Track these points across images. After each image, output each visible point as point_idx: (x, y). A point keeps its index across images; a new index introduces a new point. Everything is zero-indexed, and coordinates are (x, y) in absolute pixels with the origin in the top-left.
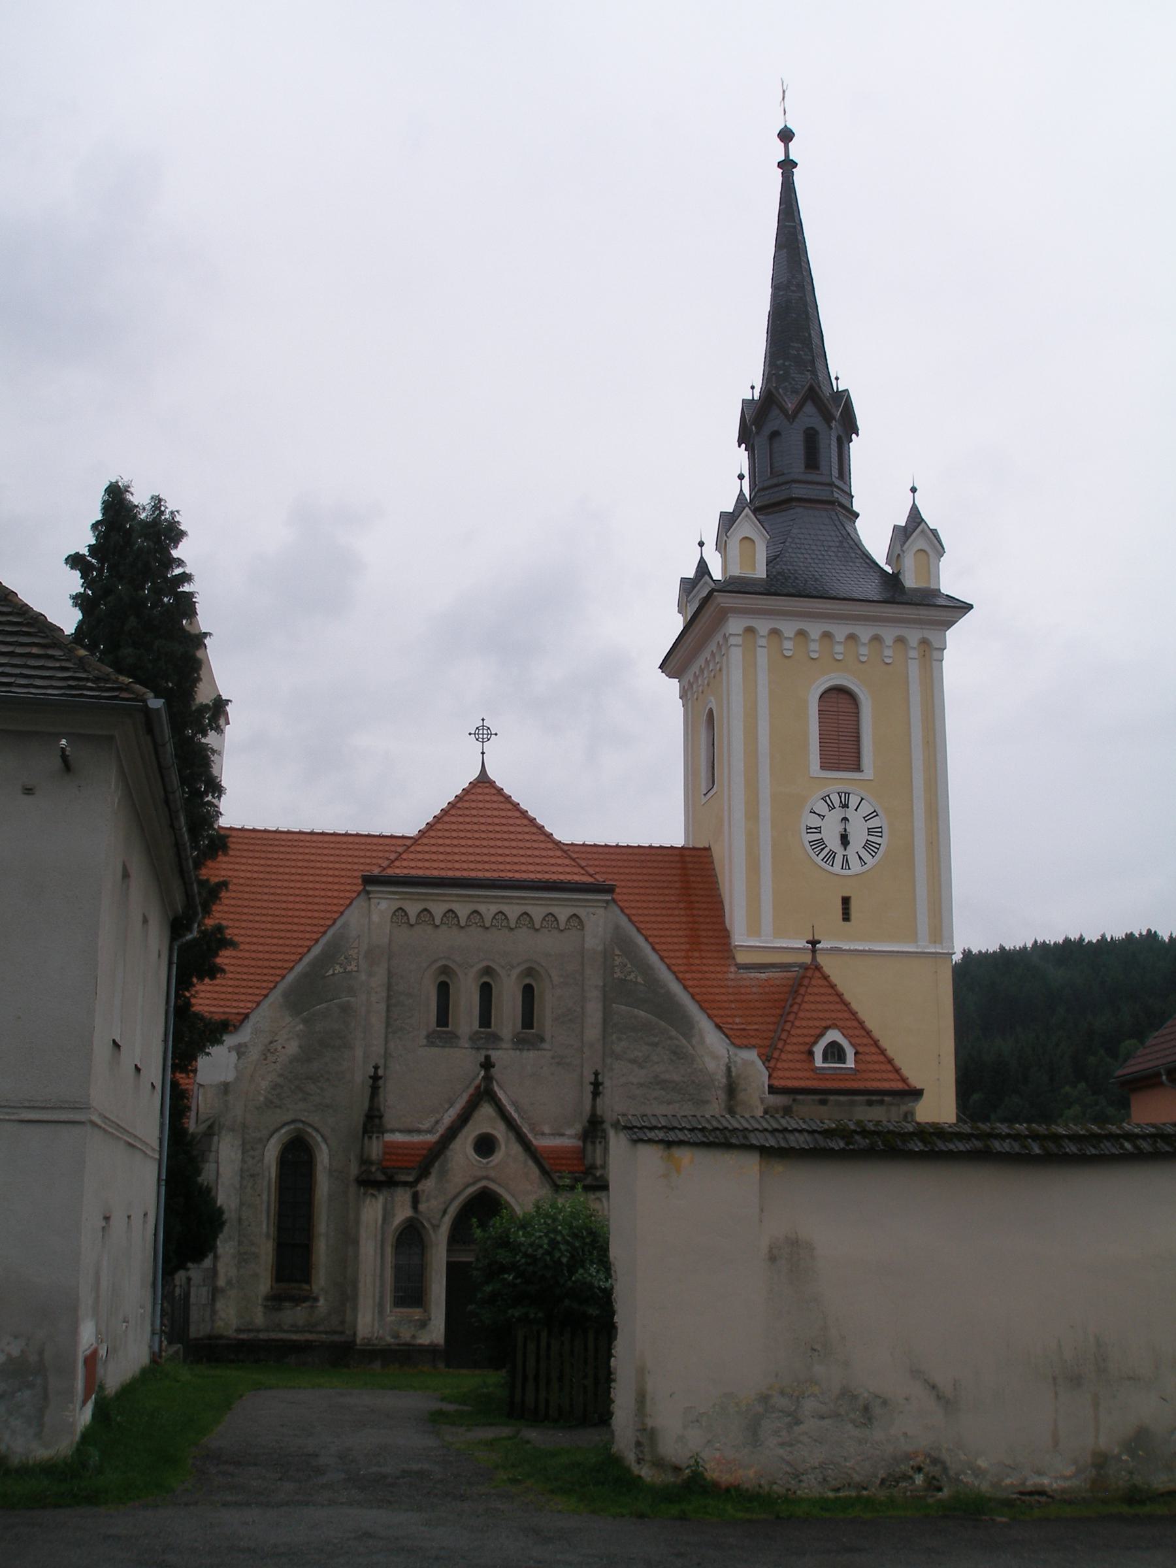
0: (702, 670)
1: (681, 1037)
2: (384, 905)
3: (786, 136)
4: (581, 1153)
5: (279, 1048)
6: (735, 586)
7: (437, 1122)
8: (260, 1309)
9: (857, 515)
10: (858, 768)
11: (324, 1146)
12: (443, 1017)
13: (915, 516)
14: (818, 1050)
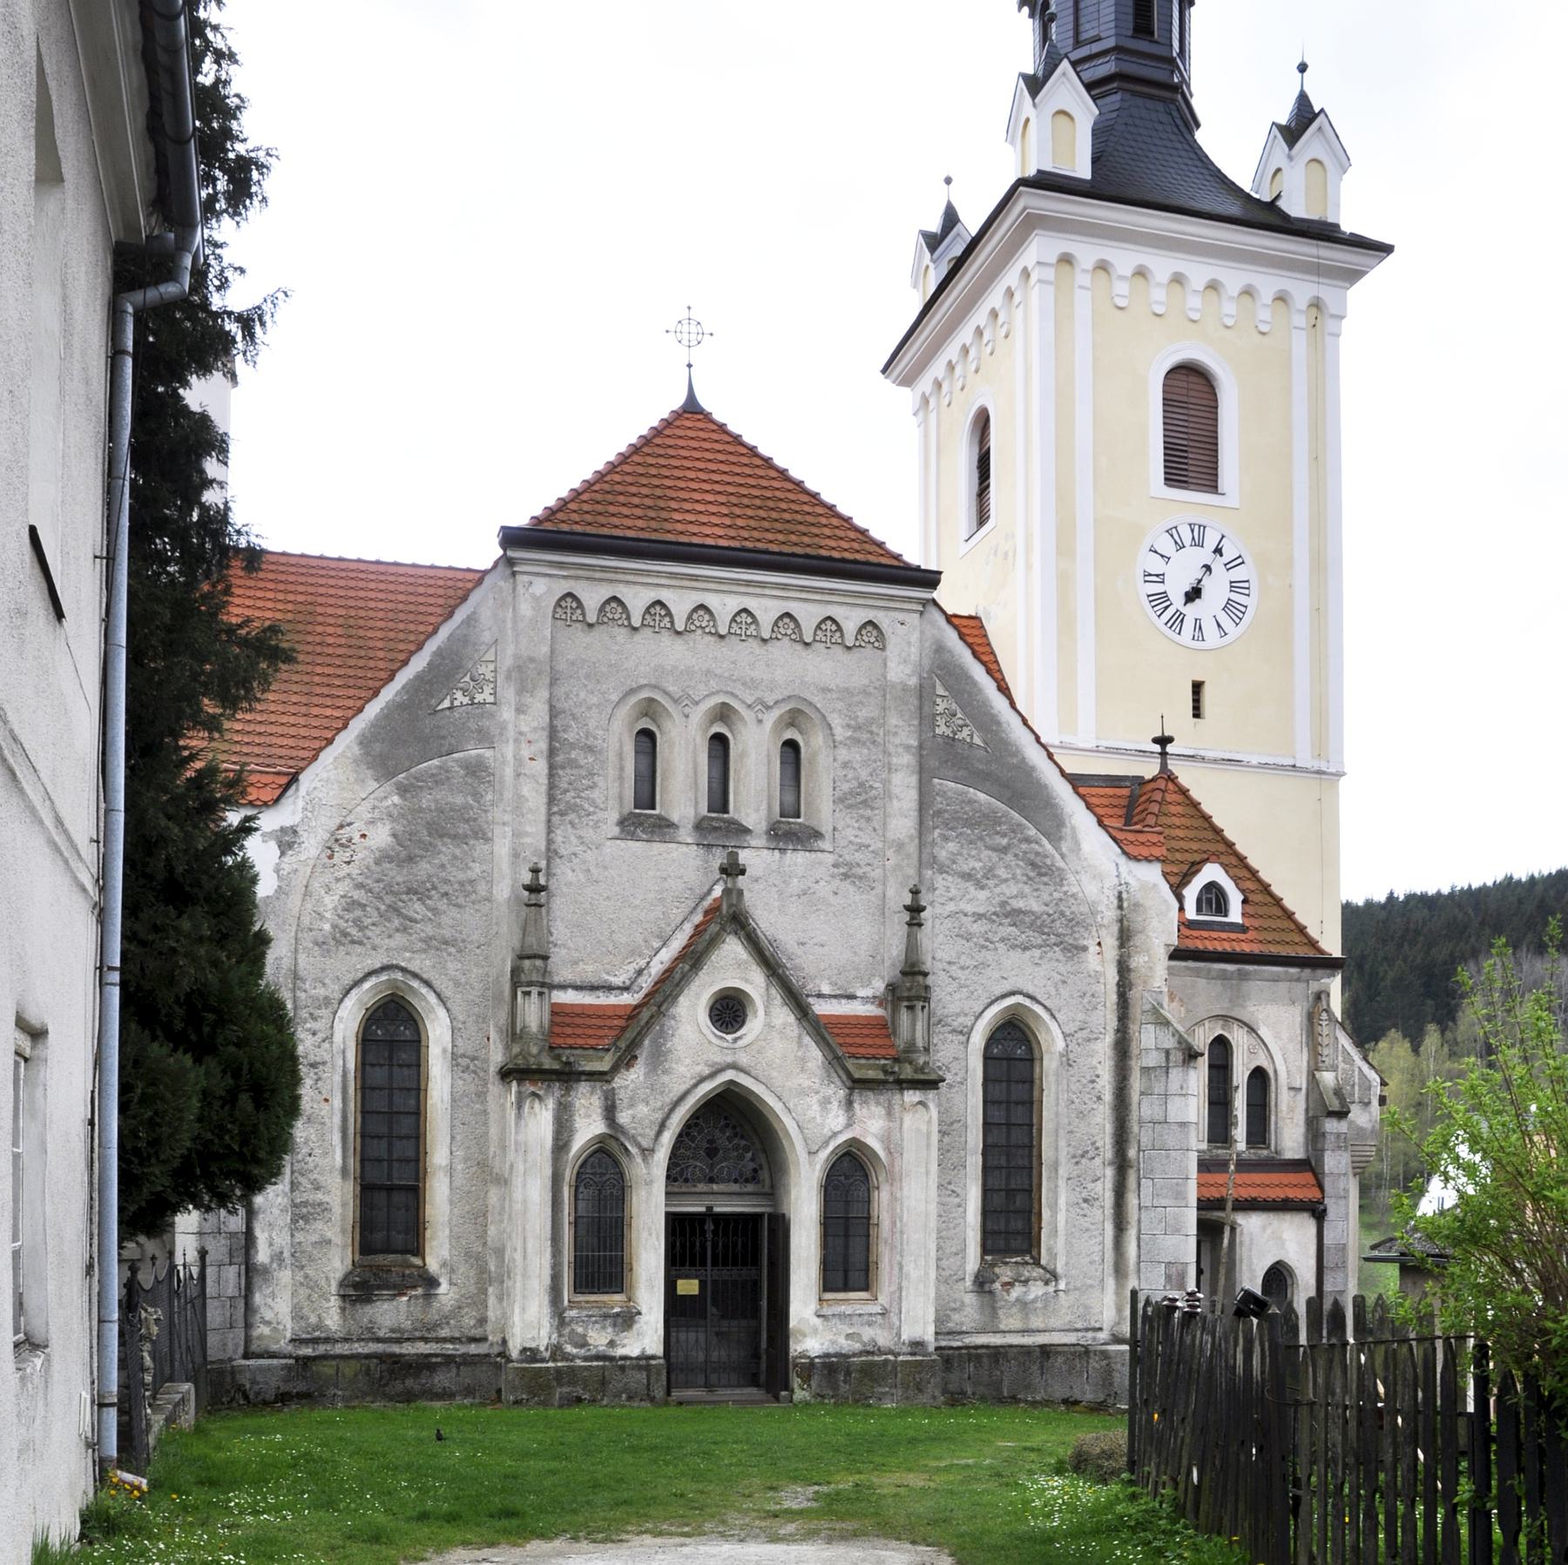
1: (1045, 841)
2: (540, 586)
5: (356, 839)
7: (640, 972)
8: (334, 1302)
11: (441, 1013)
12: (646, 793)
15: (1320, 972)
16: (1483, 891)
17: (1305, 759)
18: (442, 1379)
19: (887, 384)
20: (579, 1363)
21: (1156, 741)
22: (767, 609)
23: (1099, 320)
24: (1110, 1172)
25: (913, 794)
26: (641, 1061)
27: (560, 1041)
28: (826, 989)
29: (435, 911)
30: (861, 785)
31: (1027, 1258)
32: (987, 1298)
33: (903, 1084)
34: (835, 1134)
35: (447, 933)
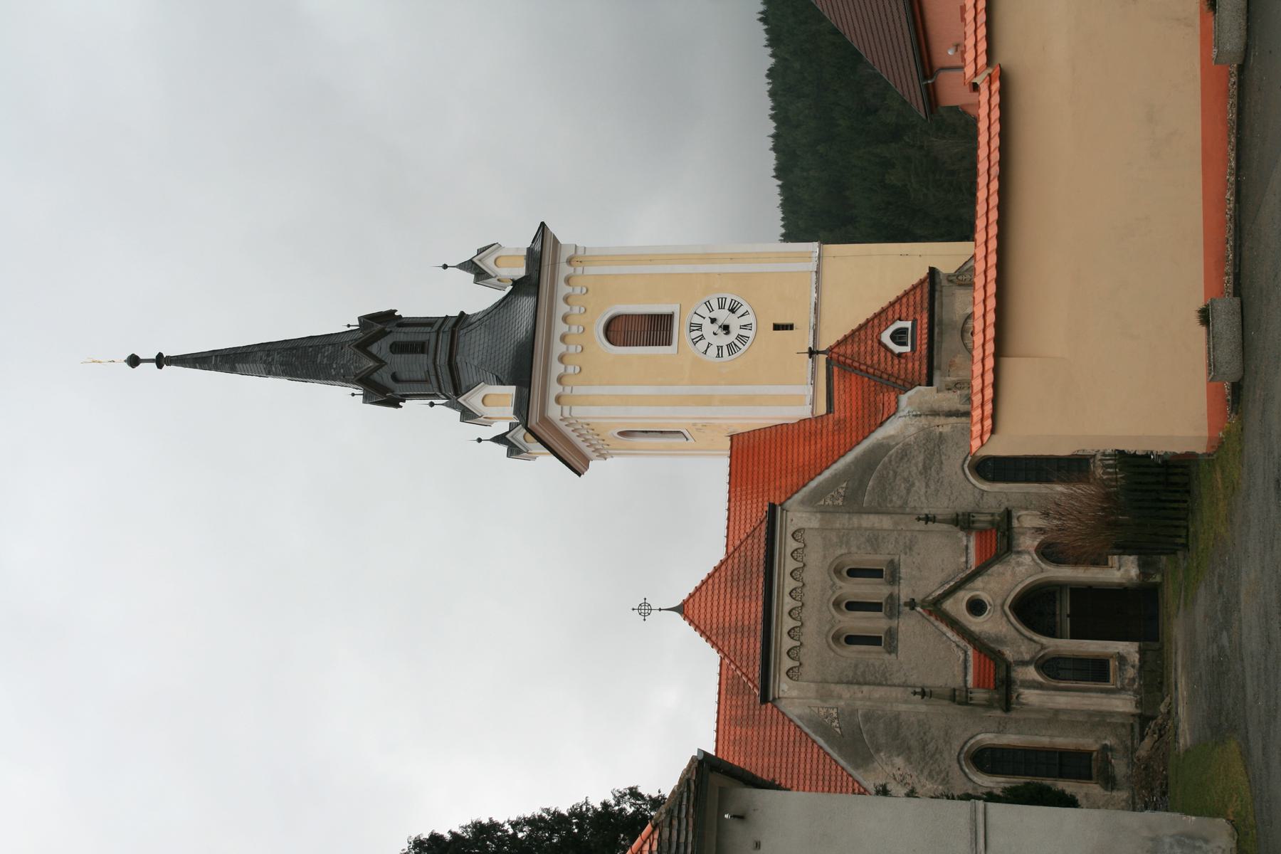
0: (586, 440)
2: (784, 687)
3: (134, 361)
4: (981, 533)
6: (522, 407)
8: (1114, 793)
9: (462, 313)
10: (669, 318)
11: (979, 737)
12: (875, 641)
13: (462, 266)
14: (898, 349)
17: (812, 266)
23: (596, 379)
25: (871, 516)
26: (1000, 648)
28: (964, 559)
29: (932, 739)
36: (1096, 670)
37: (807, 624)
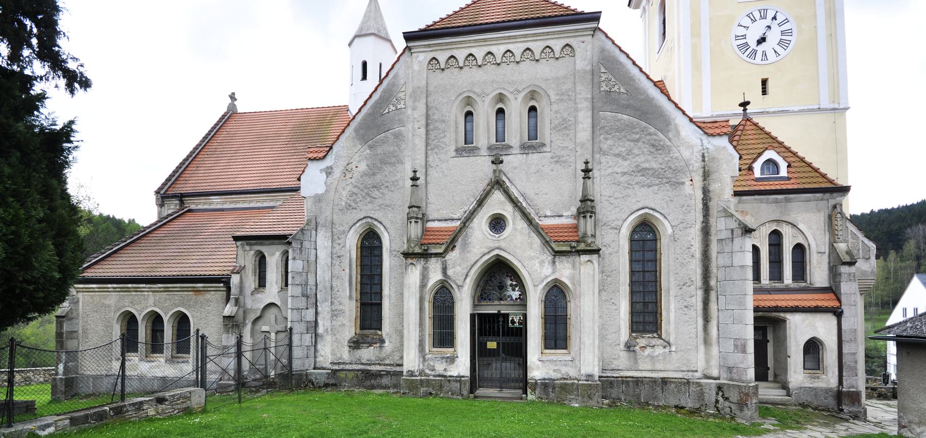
1: (660, 134)
5: (354, 168)
8: (347, 348)
11: (386, 234)
14: (757, 166)
15: (835, 195)
16: (913, 205)
17: (825, 104)
18: (385, 381)
19: (631, 10)
20: (431, 378)
21: (741, 105)
22: (518, 48)
24: (700, 293)
25: (590, 120)
27: (426, 241)
28: (548, 213)
30: (564, 120)
31: (655, 335)
32: (632, 354)
33: (580, 252)
34: (547, 277)
35: (388, 202)
36: (444, 336)
37: (480, 71)
